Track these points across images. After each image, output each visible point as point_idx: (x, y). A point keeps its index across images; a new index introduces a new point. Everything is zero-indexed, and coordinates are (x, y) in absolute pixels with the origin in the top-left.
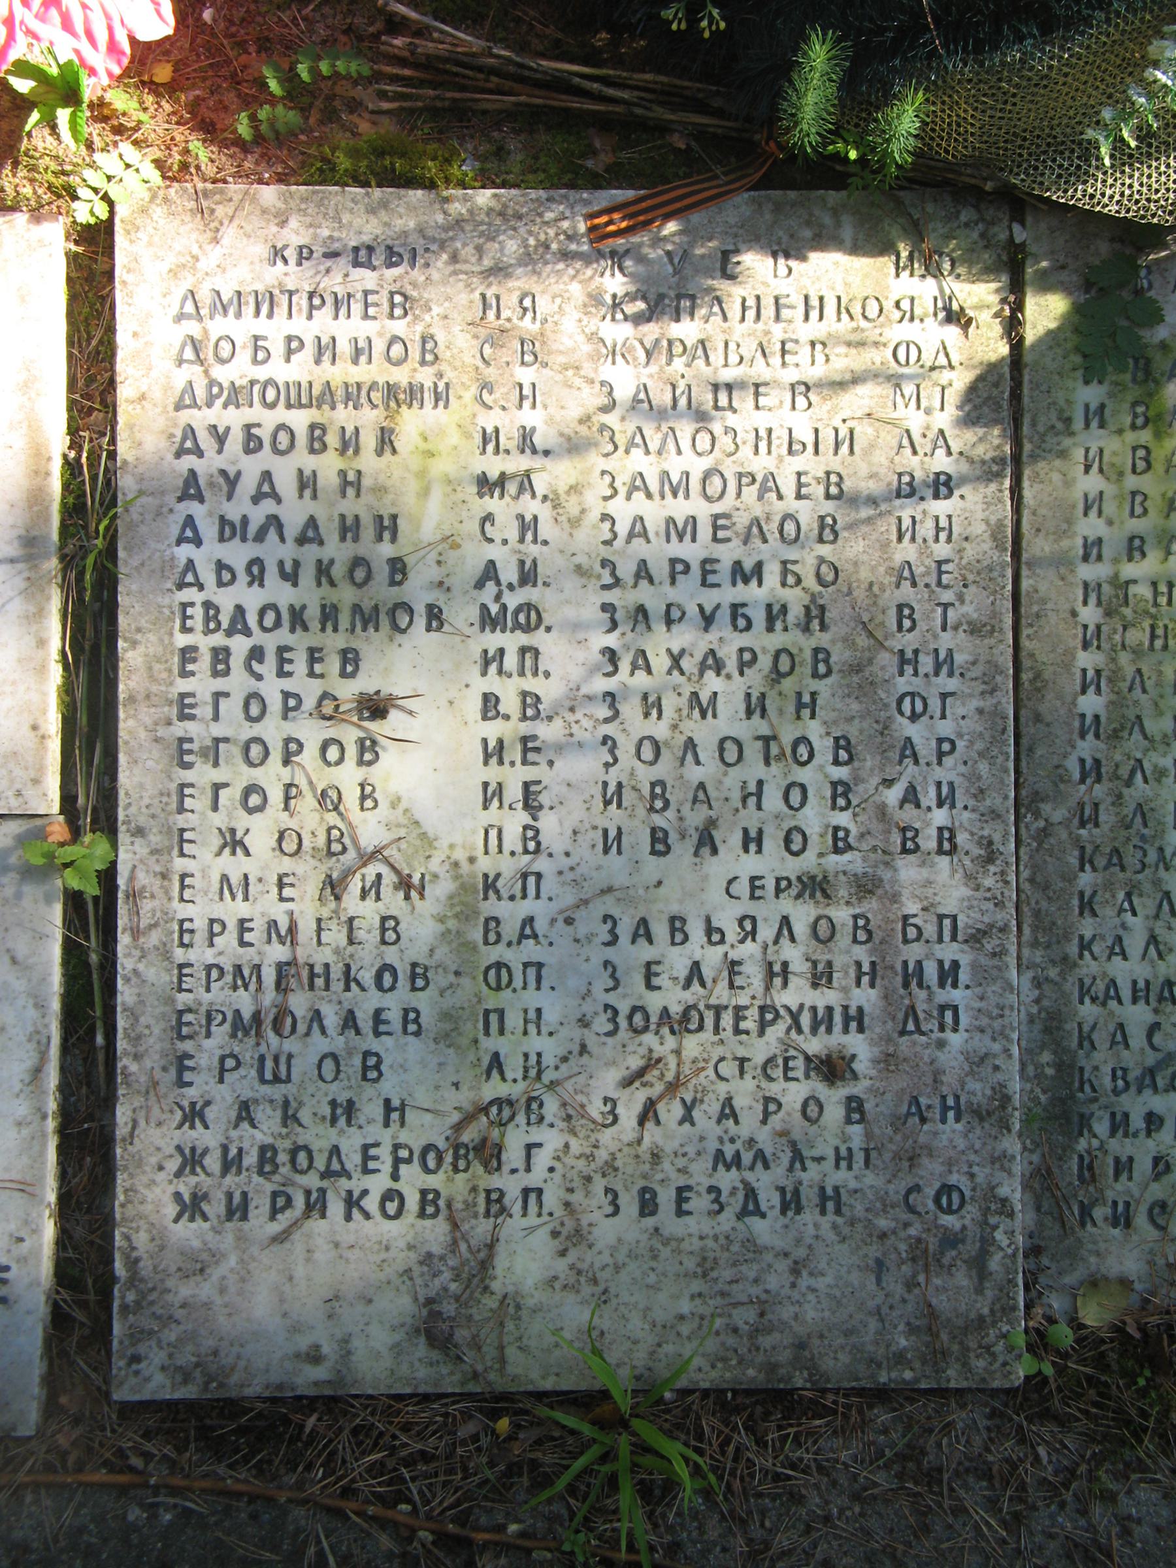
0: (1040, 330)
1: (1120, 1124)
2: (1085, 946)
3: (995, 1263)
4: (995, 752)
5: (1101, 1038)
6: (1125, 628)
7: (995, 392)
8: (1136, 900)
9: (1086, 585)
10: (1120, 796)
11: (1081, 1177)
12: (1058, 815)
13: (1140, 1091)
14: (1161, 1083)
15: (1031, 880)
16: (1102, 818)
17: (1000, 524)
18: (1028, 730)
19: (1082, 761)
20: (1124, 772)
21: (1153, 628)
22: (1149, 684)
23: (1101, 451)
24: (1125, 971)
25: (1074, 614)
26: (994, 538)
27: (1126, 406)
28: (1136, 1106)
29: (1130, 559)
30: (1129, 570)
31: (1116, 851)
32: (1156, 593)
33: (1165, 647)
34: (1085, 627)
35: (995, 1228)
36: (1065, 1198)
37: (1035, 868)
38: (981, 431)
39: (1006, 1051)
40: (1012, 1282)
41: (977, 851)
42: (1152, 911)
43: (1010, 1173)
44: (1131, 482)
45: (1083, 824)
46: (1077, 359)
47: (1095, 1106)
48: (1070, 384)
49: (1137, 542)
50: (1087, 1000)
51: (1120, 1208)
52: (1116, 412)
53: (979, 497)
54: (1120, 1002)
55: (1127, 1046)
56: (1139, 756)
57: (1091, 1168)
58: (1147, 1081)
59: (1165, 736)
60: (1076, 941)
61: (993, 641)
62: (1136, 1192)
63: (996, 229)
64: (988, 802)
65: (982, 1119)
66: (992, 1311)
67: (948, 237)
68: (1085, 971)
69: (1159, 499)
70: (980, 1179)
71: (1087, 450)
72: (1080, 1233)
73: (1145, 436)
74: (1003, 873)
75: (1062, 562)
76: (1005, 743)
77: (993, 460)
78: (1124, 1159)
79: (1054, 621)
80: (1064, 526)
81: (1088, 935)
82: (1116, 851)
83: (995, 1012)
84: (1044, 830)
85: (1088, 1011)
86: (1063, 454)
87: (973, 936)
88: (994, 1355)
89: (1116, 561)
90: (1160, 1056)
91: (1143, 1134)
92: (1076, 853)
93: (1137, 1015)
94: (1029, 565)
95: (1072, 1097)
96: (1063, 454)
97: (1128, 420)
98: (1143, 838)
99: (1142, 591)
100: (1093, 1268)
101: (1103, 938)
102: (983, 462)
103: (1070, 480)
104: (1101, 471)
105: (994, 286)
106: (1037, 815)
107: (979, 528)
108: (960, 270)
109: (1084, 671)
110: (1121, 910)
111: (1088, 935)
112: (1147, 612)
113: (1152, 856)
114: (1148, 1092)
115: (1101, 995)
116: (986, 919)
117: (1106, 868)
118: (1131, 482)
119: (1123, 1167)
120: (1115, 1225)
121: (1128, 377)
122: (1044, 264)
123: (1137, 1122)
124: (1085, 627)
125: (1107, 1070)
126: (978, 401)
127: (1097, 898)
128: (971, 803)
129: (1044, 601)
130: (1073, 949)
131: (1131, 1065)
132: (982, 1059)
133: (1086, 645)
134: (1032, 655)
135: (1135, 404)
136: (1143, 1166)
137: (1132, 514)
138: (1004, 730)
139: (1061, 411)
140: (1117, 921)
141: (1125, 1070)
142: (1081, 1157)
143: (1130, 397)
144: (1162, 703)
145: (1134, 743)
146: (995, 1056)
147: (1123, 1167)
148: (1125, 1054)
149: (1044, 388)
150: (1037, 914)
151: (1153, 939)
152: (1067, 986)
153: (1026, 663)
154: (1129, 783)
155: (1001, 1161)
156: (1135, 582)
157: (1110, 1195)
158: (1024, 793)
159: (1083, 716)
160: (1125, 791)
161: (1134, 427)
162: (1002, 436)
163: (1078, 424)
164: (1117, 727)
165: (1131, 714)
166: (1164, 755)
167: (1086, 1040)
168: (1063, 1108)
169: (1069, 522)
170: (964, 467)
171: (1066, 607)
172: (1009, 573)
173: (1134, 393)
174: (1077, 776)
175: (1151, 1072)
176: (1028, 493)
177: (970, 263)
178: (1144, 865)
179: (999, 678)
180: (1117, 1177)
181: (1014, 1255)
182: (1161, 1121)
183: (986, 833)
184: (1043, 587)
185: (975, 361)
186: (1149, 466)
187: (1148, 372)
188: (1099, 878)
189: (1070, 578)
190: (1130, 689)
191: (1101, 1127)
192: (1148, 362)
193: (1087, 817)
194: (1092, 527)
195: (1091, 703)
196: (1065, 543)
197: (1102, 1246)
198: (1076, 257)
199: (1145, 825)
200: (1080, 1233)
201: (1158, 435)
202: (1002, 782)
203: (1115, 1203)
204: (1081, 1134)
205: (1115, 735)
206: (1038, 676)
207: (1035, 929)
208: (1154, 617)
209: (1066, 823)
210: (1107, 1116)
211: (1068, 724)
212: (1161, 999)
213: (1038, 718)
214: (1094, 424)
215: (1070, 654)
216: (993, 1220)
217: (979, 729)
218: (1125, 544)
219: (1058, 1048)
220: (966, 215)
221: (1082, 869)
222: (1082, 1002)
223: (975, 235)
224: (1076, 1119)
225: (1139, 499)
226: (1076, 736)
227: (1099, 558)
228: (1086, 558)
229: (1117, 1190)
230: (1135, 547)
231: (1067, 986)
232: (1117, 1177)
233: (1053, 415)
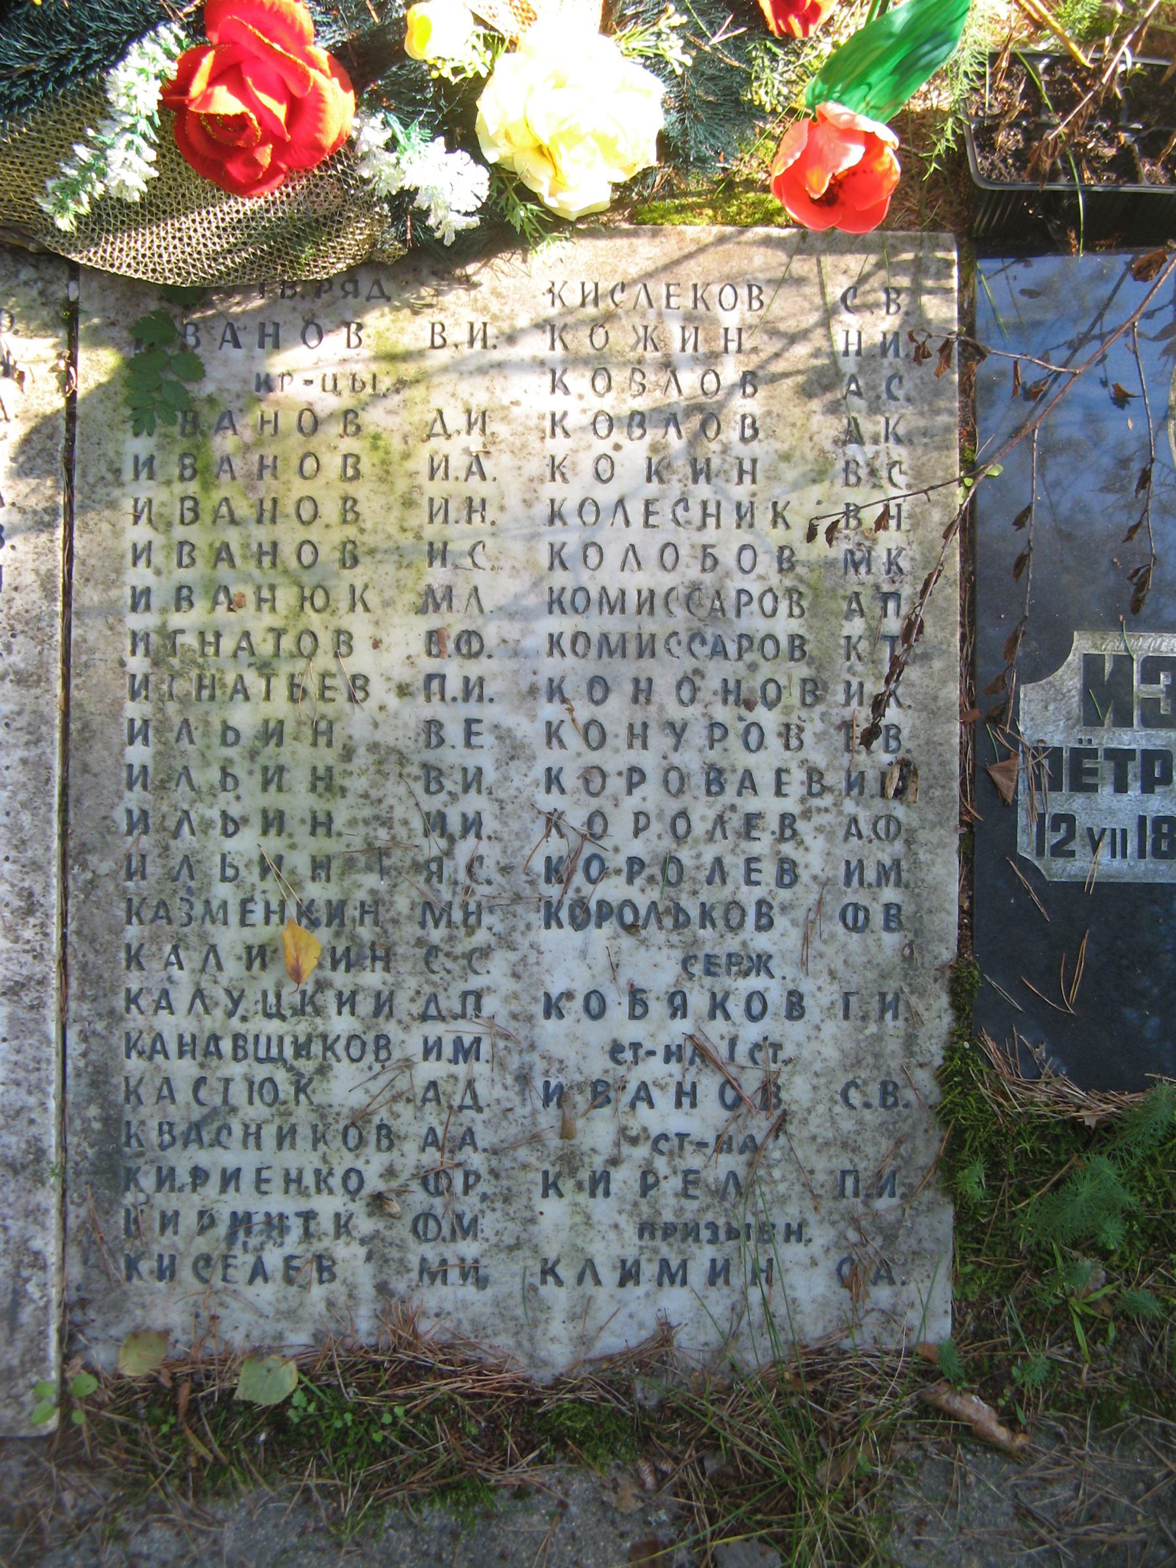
0: (92, 384)
1: (166, 1178)
2: (132, 999)
3: (26, 1315)
4: (38, 802)
5: (147, 1093)
6: (173, 678)
7: (49, 444)
8: (182, 953)
9: (134, 635)
10: (166, 848)
11: (127, 1230)
12: (105, 867)
13: (185, 1145)
14: (206, 1138)
15: (78, 933)
16: (149, 869)
17: (50, 575)
18: (75, 781)
19: (129, 812)
20: (171, 823)
21: (200, 678)
22: (196, 735)
23: (150, 501)
24: (171, 1025)
25: (122, 664)
26: (43, 587)
27: (175, 458)
28: (182, 1161)
29: (178, 609)
30: (177, 620)
31: (162, 904)
32: (203, 643)
33: (212, 698)
34: (133, 676)
35: (27, 1280)
36: (108, 1253)
37: (82, 920)
38: (33, 482)
39: (42, 1104)
40: (43, 1334)
41: (17, 903)
42: (198, 965)
43: (44, 1227)
44: (180, 532)
45: (130, 876)
46: (128, 412)
47: (141, 1161)
48: (120, 436)
49: (185, 592)
50: (134, 1054)
51: (166, 1262)
52: (164, 464)
53: (29, 548)
54: (167, 1057)
55: (173, 1100)
56: (186, 807)
57: (136, 1221)
58: (193, 1136)
59: (212, 787)
60: (123, 995)
61: (38, 691)
62: (181, 1246)
63: (54, 288)
64: (30, 854)
65: (16, 1172)
66: (22, 1363)
67: (8, 294)
68: (131, 1025)
69: (206, 549)
70: (14, 1232)
71: (136, 501)
72: (126, 1286)
73: (193, 487)
74: (42, 925)
75: (110, 611)
76: (49, 794)
77: (45, 510)
78: (170, 1213)
79: (102, 672)
80: (113, 576)
81: (135, 988)
82: (162, 904)
83: (32, 1065)
84: (91, 882)
85: (135, 1065)
86: (113, 505)
87: (10, 988)
88: (22, 1405)
89: (164, 611)
90: (205, 1110)
91: (189, 1188)
92: (124, 905)
93: (184, 1070)
94: (77, 614)
95: (119, 1151)
96: (113, 505)
97: (177, 471)
98: (189, 890)
99: (190, 640)
100: (139, 1320)
101: (149, 991)
102: (35, 512)
103: (119, 528)
104: (150, 521)
105: (52, 341)
106: (84, 866)
107: (29, 578)
108: (18, 326)
109: (132, 721)
110: (168, 964)
111: (135, 988)
112: (194, 662)
113: (199, 909)
114: (193, 1147)
115: (147, 1049)
116: (25, 972)
117: (152, 921)
118: (180, 532)
119: (169, 1221)
120: (161, 1278)
121: (176, 429)
122: (96, 321)
123: (183, 1176)
124: (133, 676)
125: (154, 1124)
126: (32, 453)
127: (144, 952)
128: (13, 854)
129: (92, 651)
130: (120, 1002)
131: (177, 1120)
132: (18, 1112)
133: (134, 695)
134: (80, 705)
135: (184, 455)
136: (189, 1220)
137: (180, 564)
138: (48, 781)
139: (111, 462)
140: (163, 974)
141: (171, 1125)
142: (128, 1212)
143: (178, 450)
144: (208, 754)
145: (181, 794)
146: (30, 1109)
147: (169, 1221)
148: (171, 1108)
149: (95, 440)
150: (84, 967)
151: (199, 993)
152: (114, 1040)
153: (74, 713)
154: (176, 835)
155: (34, 1214)
156: (182, 631)
157: (156, 1249)
158: (71, 844)
159: (130, 766)
160: (172, 843)
161: (182, 478)
162: (56, 487)
163: (128, 475)
164: (162, 779)
165: (178, 765)
166: (211, 806)
167: (132, 1093)
168: (107, 1161)
169: (118, 571)
170: (16, 517)
171: (115, 653)
172: (59, 622)
173: (183, 444)
174: (124, 827)
175: (197, 1127)
176: (77, 544)
177: (28, 319)
178: (190, 919)
179: (44, 729)
180: (163, 1228)
181: (46, 1307)
182: (207, 1176)
183: (26, 884)
184: (92, 636)
185: (31, 414)
186: (197, 517)
187: (195, 423)
188: (146, 930)
189: (119, 628)
190: (178, 740)
191: (148, 1181)
192: (196, 416)
193: (133, 869)
194: (140, 576)
195: (138, 754)
196: (114, 593)
197: (148, 1299)
198: (127, 315)
199: (192, 878)
200: (126, 1286)
201: (206, 487)
202: (44, 833)
203: (161, 1257)
204: (127, 1188)
205: (163, 786)
206: (86, 727)
207: (82, 981)
208: (201, 667)
209: (112, 875)
210: (154, 1171)
211: (115, 775)
212: (207, 1053)
213: (85, 769)
214: (144, 475)
215: (118, 704)
216: (25, 1273)
217: (23, 779)
218: (173, 593)
219: (106, 1103)
220: (26, 274)
221: (129, 922)
222: (128, 1056)
223: (34, 293)
224: (122, 1174)
225: (186, 549)
226: (123, 787)
227: (148, 607)
228: (134, 608)
229: (162, 1244)
230: (182, 597)
231: (114, 1040)
232: (163, 1228)
233: (103, 467)
